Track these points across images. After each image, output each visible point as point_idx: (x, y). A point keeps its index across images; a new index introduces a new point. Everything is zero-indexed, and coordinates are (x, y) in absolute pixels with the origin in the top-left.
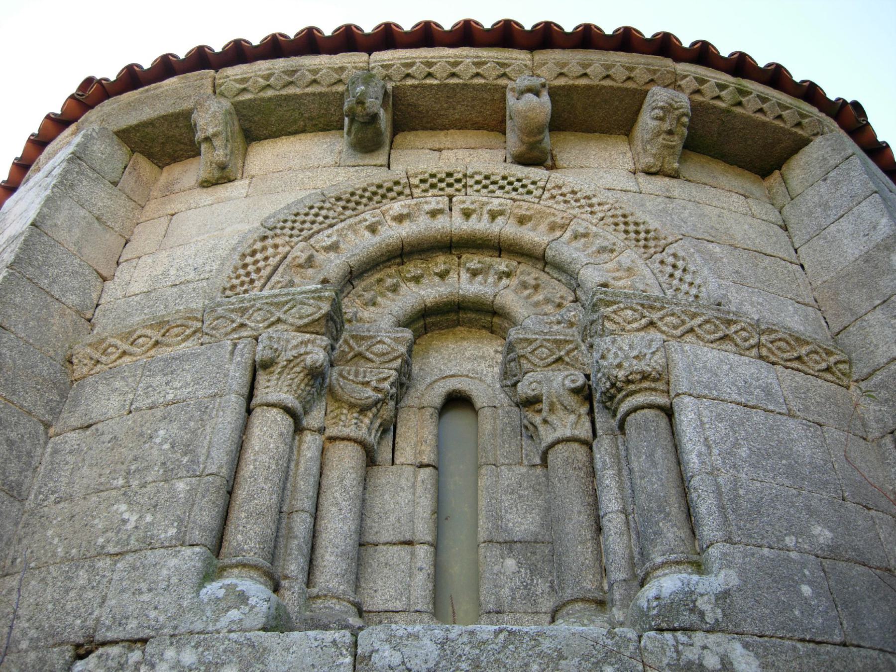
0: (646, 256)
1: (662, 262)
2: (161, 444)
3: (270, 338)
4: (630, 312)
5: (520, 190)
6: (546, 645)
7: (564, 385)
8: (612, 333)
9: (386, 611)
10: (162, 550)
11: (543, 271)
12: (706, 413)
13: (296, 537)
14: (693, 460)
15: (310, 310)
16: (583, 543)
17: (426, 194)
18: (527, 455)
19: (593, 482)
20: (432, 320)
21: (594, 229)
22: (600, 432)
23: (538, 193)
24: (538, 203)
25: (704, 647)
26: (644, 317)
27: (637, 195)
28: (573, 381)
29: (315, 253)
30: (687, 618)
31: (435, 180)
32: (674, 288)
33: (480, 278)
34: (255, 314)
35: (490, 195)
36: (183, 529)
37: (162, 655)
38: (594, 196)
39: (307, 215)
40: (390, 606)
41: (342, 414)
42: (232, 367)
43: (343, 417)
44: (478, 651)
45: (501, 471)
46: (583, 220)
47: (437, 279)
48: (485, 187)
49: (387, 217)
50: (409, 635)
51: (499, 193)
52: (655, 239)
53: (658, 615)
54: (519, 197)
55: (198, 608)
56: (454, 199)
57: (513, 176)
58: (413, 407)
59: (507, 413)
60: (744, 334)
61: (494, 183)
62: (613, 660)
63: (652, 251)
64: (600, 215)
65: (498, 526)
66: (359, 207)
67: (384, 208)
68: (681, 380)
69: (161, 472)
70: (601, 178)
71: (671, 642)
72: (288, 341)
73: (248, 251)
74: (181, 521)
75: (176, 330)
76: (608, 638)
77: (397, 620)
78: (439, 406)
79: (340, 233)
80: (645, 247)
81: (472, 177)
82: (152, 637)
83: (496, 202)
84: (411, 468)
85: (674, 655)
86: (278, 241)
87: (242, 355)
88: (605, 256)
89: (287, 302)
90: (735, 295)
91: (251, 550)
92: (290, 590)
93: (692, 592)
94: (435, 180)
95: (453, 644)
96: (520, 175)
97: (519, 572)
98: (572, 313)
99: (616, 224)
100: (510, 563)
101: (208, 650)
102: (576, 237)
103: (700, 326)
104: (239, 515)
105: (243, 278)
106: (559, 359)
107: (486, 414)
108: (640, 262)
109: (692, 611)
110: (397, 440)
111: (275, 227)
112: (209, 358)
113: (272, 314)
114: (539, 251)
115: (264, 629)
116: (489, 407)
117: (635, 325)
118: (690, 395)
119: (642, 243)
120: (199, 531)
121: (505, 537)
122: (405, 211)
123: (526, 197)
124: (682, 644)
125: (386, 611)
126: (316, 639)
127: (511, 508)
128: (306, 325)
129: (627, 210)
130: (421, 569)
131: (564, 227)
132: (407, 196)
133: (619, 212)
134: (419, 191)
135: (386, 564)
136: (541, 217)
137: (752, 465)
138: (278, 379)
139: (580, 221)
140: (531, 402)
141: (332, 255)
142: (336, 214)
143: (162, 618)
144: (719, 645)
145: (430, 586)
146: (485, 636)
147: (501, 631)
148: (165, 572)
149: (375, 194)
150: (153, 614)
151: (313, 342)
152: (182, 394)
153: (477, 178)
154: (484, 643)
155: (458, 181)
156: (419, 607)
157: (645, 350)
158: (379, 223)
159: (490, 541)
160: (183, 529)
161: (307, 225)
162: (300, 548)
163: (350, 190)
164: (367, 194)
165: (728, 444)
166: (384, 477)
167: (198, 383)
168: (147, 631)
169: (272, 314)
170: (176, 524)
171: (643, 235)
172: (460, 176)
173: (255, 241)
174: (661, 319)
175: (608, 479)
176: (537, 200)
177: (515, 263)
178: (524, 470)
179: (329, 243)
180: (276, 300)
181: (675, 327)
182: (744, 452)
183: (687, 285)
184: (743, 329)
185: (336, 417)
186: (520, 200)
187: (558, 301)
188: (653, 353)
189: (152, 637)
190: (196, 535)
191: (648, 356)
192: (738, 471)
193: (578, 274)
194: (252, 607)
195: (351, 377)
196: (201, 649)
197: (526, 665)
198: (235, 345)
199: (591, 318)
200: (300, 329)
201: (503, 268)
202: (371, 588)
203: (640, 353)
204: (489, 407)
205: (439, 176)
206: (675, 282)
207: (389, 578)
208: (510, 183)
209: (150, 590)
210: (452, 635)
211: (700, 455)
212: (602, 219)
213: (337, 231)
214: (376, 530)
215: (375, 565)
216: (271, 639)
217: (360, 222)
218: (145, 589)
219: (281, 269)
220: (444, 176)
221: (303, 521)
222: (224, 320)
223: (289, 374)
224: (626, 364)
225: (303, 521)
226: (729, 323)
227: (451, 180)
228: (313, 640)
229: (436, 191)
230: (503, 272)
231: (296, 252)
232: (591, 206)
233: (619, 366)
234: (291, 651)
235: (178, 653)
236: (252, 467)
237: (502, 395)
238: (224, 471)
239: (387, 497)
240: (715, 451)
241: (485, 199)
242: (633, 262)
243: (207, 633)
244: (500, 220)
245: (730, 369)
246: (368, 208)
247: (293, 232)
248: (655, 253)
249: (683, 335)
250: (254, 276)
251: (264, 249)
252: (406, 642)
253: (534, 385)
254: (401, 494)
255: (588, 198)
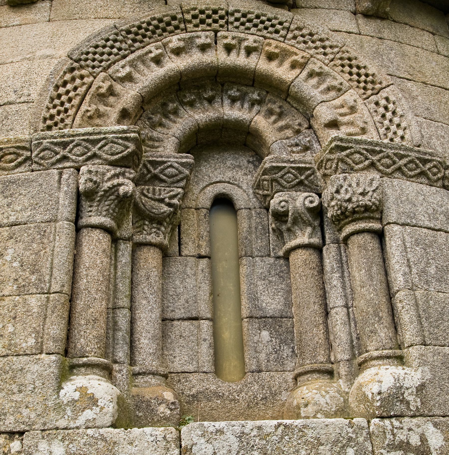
0: (365, 96)
1: (377, 104)
2: (11, 262)
3: (90, 172)
4: (358, 156)
5: (270, 29)
6: (310, 433)
7: (304, 204)
8: (344, 172)
9: (183, 372)
10: (26, 357)
11: (286, 100)
12: (407, 238)
13: (120, 330)
14: (398, 279)
15: (120, 148)
16: (317, 326)
17: (197, 29)
18: (274, 249)
19: (322, 278)
20: (205, 142)
21: (326, 68)
22: (328, 241)
23: (283, 32)
24: (284, 42)
25: (410, 430)
26: (368, 159)
27: (357, 36)
28: (311, 202)
29: (114, 83)
30: (399, 408)
31: (203, 16)
32: (385, 127)
33: (238, 104)
34: (75, 149)
35: (246, 32)
36: (40, 340)
37: (37, 447)
38: (328, 39)
39: (104, 47)
40: (186, 368)
41: (145, 224)
42: (62, 195)
43: (146, 228)
44: (264, 442)
45: (256, 262)
46: (318, 59)
47: (206, 104)
48: (243, 24)
49: (167, 49)
50: (217, 431)
51: (253, 30)
52: (373, 82)
53: (380, 407)
54: (268, 35)
55: (59, 408)
56: (219, 34)
57: (265, 15)
58: (191, 208)
59: (259, 214)
60: (435, 170)
61: (250, 21)
62: (353, 444)
63: (369, 92)
64: (332, 56)
65: (256, 305)
66: (145, 40)
67: (165, 41)
68: (392, 215)
69: (15, 287)
70: (331, 19)
71: (390, 427)
72: (104, 174)
73: (60, 83)
74: (38, 332)
75: (9, 157)
76: (349, 427)
77: (191, 379)
78: (209, 207)
79: (132, 64)
80: (365, 88)
81: (232, 14)
82: (28, 431)
83: (251, 38)
84: (193, 259)
85: (391, 437)
86: (84, 72)
87: (68, 186)
88: (333, 94)
89: (100, 140)
90: (426, 130)
91: (92, 351)
92: (120, 373)
93: (401, 387)
94: (203, 16)
95: (248, 437)
96: (270, 15)
97: (271, 341)
98: (308, 139)
99: (343, 66)
100: (265, 334)
101: (72, 443)
102: (311, 75)
103: (405, 165)
104: (81, 321)
105: (59, 108)
106: (301, 183)
107: (243, 213)
108: (360, 101)
109: (401, 401)
110: (182, 236)
111: (80, 60)
112: (41, 185)
113: (89, 150)
114: (284, 87)
115: (114, 426)
116: (245, 208)
117: (361, 166)
118: (398, 224)
119: (362, 85)
120: (53, 342)
121: (260, 313)
122: (182, 44)
123: (274, 35)
124: (396, 428)
125: (183, 372)
126: (151, 435)
127: (264, 291)
128: (116, 160)
129: (353, 54)
130: (205, 340)
131: (303, 66)
132: (182, 30)
133: (346, 55)
134: (191, 26)
135: (181, 336)
136: (286, 55)
137: (438, 280)
138: (98, 206)
139: (316, 61)
140: (281, 217)
141: (128, 85)
142: (127, 46)
143: (33, 415)
144: (419, 426)
145: (212, 351)
146: (269, 430)
147: (279, 425)
148: (29, 376)
149: (157, 27)
150: (25, 412)
151: (123, 174)
152: (24, 216)
153: (237, 15)
154: (268, 435)
155: (222, 17)
156: (205, 370)
157: (368, 189)
158: (161, 55)
159: (251, 317)
160: (40, 340)
161: (105, 57)
162: (124, 340)
163: (137, 23)
164: (151, 28)
165: (423, 265)
166: (176, 267)
167: (35, 208)
168: (23, 426)
169: (89, 150)
170: (33, 335)
171: (363, 78)
172: (223, 12)
173: (65, 73)
174: (379, 161)
175: (334, 280)
176: (282, 39)
177: (264, 93)
178: (272, 260)
179: (124, 74)
180: (91, 137)
181: (388, 167)
182: (432, 270)
183: (395, 126)
184: (435, 166)
185: (140, 226)
186: (269, 38)
187: (297, 127)
188: (374, 191)
189: (28, 431)
190: (50, 345)
191: (370, 194)
192: (429, 286)
193: (314, 109)
194: (102, 408)
195: (150, 195)
196: (67, 443)
197: (298, 451)
198: (61, 174)
199: (329, 156)
200: (113, 164)
201: (255, 96)
202: (171, 355)
203: (365, 190)
204: (245, 208)
205: (207, 12)
206: (386, 122)
207: (183, 346)
208: (262, 22)
209: (20, 391)
210: (247, 431)
211: (405, 274)
212: (332, 60)
213: (129, 62)
214: (171, 308)
215: (173, 337)
216: (118, 433)
217: (147, 53)
218: (15, 390)
219: (88, 98)
220: (210, 12)
221: (125, 316)
222: (49, 152)
223: (105, 201)
224: (354, 199)
225: (125, 316)
226: (425, 162)
227: (216, 17)
228: (149, 436)
229: (204, 26)
230: (256, 100)
231: (98, 82)
232: (324, 47)
233: (349, 200)
234: (134, 444)
235: (50, 445)
236: (85, 281)
237: (254, 199)
238: (66, 289)
239: (177, 282)
240: (414, 271)
241: (242, 35)
242: (355, 101)
243: (70, 429)
244: (254, 56)
245: (424, 199)
246: (152, 40)
247: (95, 63)
248: (372, 94)
249: (393, 172)
250: (67, 105)
251: (73, 79)
252: (216, 437)
253: (283, 204)
254: (187, 280)
255: (321, 40)
